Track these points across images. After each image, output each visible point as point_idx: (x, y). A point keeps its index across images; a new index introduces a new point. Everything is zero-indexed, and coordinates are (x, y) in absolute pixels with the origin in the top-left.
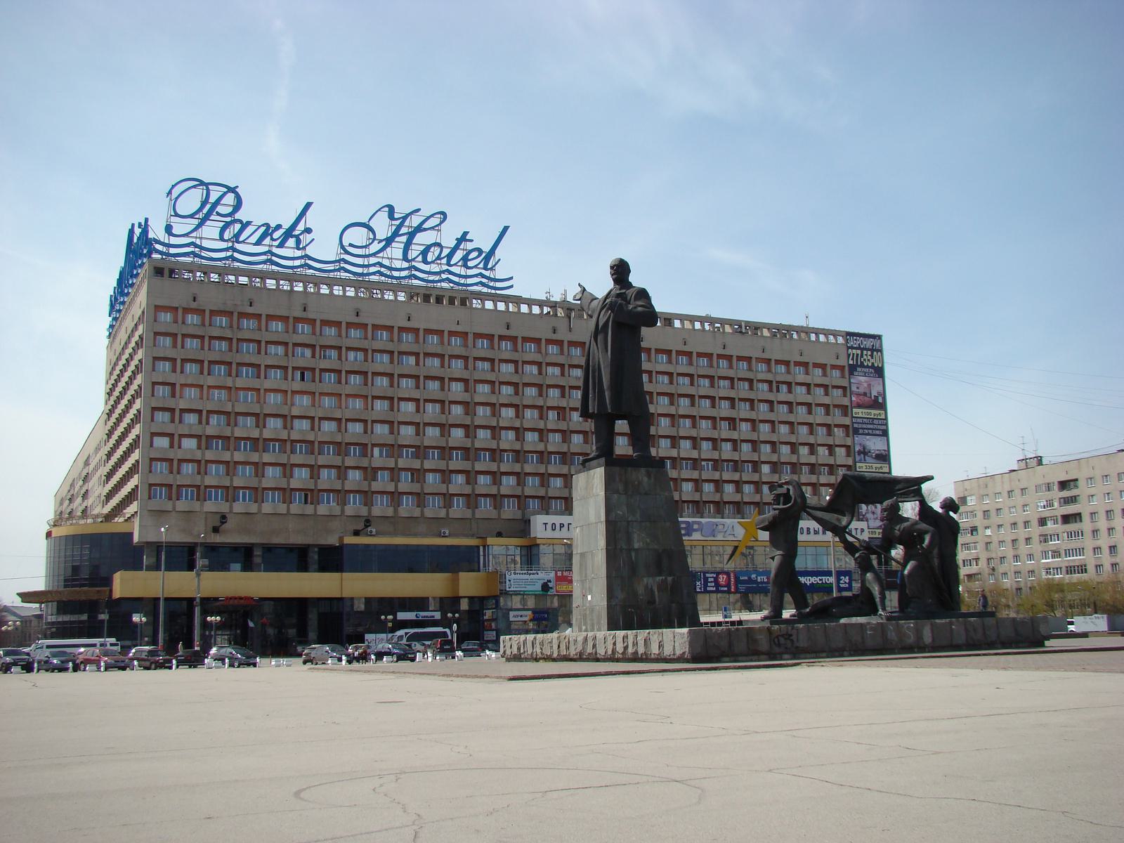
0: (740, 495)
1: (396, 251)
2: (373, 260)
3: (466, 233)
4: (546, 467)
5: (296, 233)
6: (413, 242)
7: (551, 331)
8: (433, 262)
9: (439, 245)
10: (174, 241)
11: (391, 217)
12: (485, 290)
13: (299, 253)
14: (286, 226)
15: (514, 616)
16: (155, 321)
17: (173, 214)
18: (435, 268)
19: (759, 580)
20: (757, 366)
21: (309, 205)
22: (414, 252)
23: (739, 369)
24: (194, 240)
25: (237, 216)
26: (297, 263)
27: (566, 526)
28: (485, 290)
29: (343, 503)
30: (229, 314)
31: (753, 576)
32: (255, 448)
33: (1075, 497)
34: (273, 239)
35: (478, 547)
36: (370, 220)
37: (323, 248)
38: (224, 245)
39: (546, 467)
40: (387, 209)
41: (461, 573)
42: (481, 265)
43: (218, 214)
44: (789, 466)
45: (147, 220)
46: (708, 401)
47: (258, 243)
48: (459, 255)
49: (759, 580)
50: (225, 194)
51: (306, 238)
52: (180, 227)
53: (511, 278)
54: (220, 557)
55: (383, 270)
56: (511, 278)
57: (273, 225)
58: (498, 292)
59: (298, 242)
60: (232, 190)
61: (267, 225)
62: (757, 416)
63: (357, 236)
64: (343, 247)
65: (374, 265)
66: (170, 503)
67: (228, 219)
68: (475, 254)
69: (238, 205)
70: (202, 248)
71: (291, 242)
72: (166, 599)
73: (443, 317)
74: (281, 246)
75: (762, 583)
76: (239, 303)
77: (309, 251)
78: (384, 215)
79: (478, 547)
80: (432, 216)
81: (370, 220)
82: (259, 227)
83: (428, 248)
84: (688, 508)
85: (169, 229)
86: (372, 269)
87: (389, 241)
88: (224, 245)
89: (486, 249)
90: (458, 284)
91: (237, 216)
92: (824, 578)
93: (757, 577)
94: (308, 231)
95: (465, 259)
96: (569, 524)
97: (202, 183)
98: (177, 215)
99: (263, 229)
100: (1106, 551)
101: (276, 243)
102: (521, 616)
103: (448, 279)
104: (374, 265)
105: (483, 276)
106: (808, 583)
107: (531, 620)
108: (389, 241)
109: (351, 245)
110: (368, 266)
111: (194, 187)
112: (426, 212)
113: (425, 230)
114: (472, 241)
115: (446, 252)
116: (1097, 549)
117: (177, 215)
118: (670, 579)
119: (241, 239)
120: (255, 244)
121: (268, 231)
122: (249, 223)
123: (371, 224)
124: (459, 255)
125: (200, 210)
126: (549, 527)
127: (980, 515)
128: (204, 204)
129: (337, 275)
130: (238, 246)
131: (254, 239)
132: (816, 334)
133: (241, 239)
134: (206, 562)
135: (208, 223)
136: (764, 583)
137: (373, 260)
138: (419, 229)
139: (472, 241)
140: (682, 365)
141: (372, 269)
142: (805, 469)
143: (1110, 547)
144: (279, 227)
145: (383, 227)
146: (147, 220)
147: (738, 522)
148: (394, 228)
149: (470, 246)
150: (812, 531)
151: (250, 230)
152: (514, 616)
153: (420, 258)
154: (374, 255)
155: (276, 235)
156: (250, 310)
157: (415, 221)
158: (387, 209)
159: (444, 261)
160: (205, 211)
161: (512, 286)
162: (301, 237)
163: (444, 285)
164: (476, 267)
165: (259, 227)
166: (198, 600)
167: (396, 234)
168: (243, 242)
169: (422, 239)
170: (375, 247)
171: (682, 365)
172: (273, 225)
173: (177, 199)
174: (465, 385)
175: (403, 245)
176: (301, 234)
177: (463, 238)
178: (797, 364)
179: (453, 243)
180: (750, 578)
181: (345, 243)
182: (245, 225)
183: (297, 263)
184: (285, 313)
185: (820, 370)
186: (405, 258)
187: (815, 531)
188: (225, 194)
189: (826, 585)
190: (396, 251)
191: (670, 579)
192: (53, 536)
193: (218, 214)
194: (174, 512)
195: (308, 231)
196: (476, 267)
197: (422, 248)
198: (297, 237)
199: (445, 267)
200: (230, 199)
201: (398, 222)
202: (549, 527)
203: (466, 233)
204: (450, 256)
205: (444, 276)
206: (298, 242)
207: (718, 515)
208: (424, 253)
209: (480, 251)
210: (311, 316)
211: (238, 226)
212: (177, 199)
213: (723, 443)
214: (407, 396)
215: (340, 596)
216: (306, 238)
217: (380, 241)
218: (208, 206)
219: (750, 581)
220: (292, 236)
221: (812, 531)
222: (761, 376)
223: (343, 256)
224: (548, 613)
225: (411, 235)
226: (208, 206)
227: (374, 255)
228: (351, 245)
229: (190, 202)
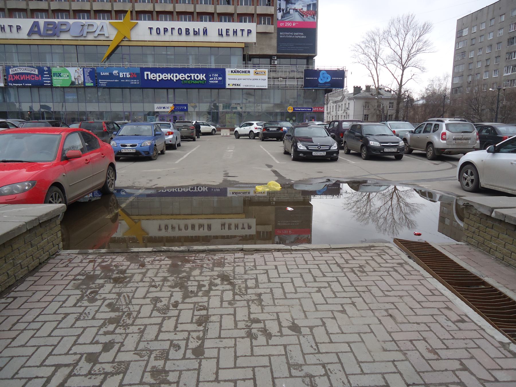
15: (158, 108)
16: (501, 16)
19: (121, 75)
27: (170, 30)
31: (115, 72)
49: (121, 75)
75: (123, 78)
92: (192, 75)
93: (119, 74)
96: (172, 28)
102: (164, 108)
126: (154, 31)
133: (120, 344)
136: (126, 78)
150: (191, 32)
152: (158, 108)
175: (196, 287)
180: (111, 74)
187: (194, 31)
189: (195, 82)
192: (349, 87)
202: (154, 31)
219: (111, 76)
221: (191, 32)
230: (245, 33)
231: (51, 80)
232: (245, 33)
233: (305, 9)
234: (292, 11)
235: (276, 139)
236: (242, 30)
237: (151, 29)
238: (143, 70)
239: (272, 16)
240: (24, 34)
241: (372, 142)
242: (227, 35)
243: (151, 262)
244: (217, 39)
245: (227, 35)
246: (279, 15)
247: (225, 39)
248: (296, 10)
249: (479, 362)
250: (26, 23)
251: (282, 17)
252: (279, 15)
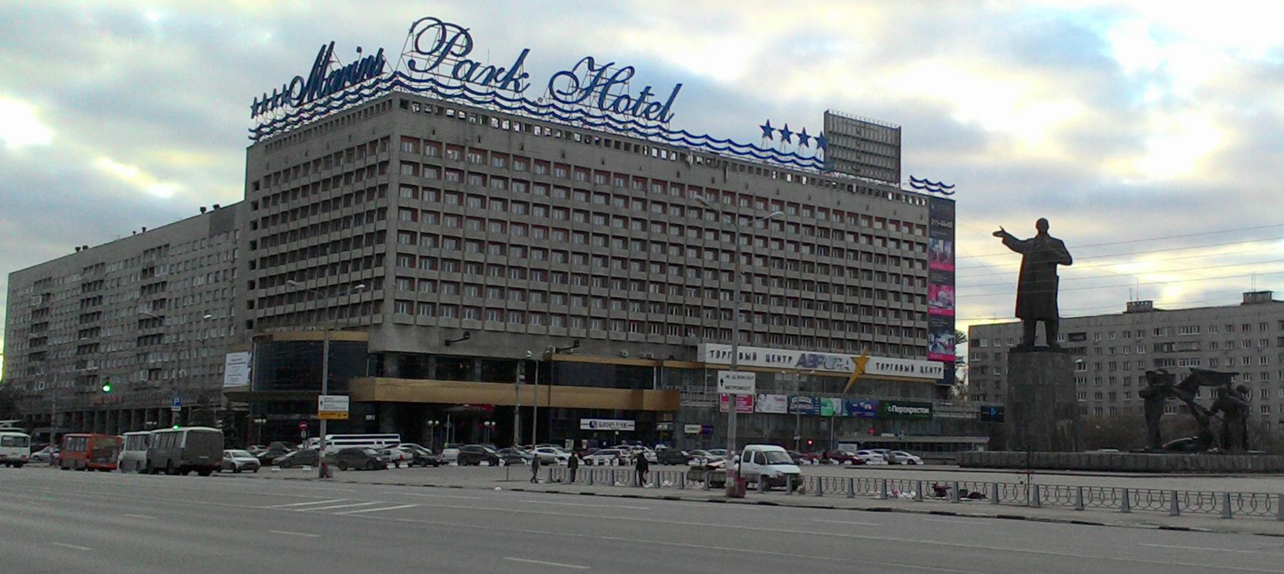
0: (750, 324)
1: (593, 100)
2: (576, 107)
3: (648, 88)
4: (463, 276)
5: (516, 77)
6: (609, 92)
7: (600, 163)
8: (623, 112)
9: (627, 97)
10: (416, 76)
11: (591, 67)
12: (660, 140)
13: (517, 96)
14: (508, 69)
17: (414, 49)
18: (620, 117)
20: (595, 178)
21: (526, 51)
22: (608, 103)
23: (404, 151)
24: (432, 76)
25: (468, 57)
26: (516, 105)
28: (660, 140)
29: (547, 324)
30: (461, 148)
31: (862, 404)
32: (479, 271)
33: (1082, 348)
34: (496, 81)
35: (652, 368)
36: (575, 69)
37: (536, 91)
38: (457, 83)
39: (463, 276)
40: (630, 70)
41: (645, 391)
42: (659, 118)
43: (453, 53)
44: (451, 264)
45: (333, 43)
46: (500, 204)
47: (484, 84)
48: (643, 106)
50: (459, 35)
51: (523, 82)
52: (421, 63)
53: (953, 186)
54: (454, 368)
55: (611, 122)
56: (953, 186)
57: (497, 68)
58: (672, 143)
59: (517, 85)
60: (464, 31)
61: (493, 67)
62: (465, 211)
63: (563, 83)
64: (552, 92)
65: (576, 111)
66: (412, 317)
67: (461, 59)
68: (655, 107)
69: (469, 47)
70: (587, 115)
71: (511, 85)
72: (538, 408)
73: (618, 161)
74: (503, 87)
76: (470, 139)
77: (526, 94)
78: (585, 65)
79: (652, 368)
80: (623, 70)
81: (575, 69)
82: (486, 69)
83: (620, 98)
84: (596, 324)
85: (412, 64)
86: (575, 115)
87: (589, 90)
88: (457, 83)
89: (663, 104)
90: (408, 87)
91: (468, 57)
94: (526, 75)
95: (647, 112)
97: (439, 22)
98: (418, 51)
99: (489, 70)
100: (1106, 396)
101: (499, 85)
103: (553, 113)
104: (576, 111)
105: (660, 127)
106: (911, 412)
107: (700, 433)
108: (589, 90)
109: (559, 92)
110: (571, 112)
111: (433, 26)
112: (618, 66)
113: (617, 82)
114: (652, 95)
115: (633, 103)
116: (1099, 395)
117: (418, 51)
118: (1071, 421)
119: (471, 79)
120: (482, 85)
121: (493, 73)
122: (478, 64)
123: (575, 73)
124: (643, 106)
125: (437, 49)
127: (991, 357)
128: (442, 41)
129: (519, 112)
130: (468, 85)
131: (481, 80)
132: (658, 150)
134: (523, 377)
135: (445, 61)
137: (576, 107)
138: (612, 80)
139: (652, 95)
140: (776, 212)
141: (575, 115)
142: (918, 316)
143: (1110, 394)
144: (502, 70)
145: (585, 79)
146: (333, 43)
147: (852, 358)
148: (593, 78)
149: (650, 99)
150: (744, 356)
151: (479, 70)
153: (612, 109)
154: (576, 102)
155: (500, 77)
156: (477, 146)
157: (609, 73)
158: (587, 60)
159: (630, 112)
160: (441, 50)
161: (953, 193)
162: (520, 81)
163: (632, 134)
164: (655, 119)
165: (486, 69)
166: (517, 409)
167: (594, 84)
168: (473, 82)
169: (615, 89)
170: (576, 96)
171: (776, 212)
172: (497, 68)
173: (419, 35)
174: (642, 225)
176: (520, 78)
177: (646, 92)
178: (774, 201)
179: (637, 96)
181: (555, 89)
182: (474, 66)
183: (516, 105)
184: (504, 150)
185: (659, 187)
186: (455, 75)
188: (459, 35)
190: (593, 100)
191: (1071, 421)
193: (453, 53)
194: (414, 327)
195: (526, 75)
196: (655, 119)
197: (615, 98)
198: (516, 80)
199: (631, 118)
200: (462, 40)
201: (595, 73)
202: (715, 354)
203: (648, 88)
204: (635, 109)
205: (630, 126)
206: (517, 85)
207: (896, 355)
208: (615, 105)
209: (658, 104)
210: (527, 155)
211: (468, 66)
212: (419, 35)
213: (671, 268)
214: (406, 206)
215: (546, 405)
216: (523, 82)
217: (582, 90)
218: (445, 45)
220: (513, 79)
222: (864, 232)
223: (553, 101)
224: (712, 427)
225: (607, 86)
226: (445, 45)
227: (576, 102)
228: (559, 92)
229: (429, 41)
230: (787, 359)
231: (820, 409)
232: (787, 359)
233: (947, 343)
234: (938, 345)
235: (585, 424)
236: (784, 357)
237: (878, 364)
238: (882, 403)
239: (924, 347)
240: (793, 365)
241: (588, 421)
242: (773, 360)
243: (730, 481)
244: (764, 364)
245: (773, 360)
246: (930, 347)
247: (771, 364)
248: (940, 343)
249: (965, 516)
250: (796, 355)
251: (933, 349)
252: (930, 347)
